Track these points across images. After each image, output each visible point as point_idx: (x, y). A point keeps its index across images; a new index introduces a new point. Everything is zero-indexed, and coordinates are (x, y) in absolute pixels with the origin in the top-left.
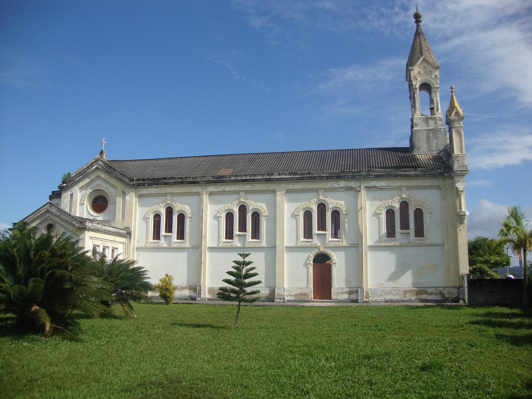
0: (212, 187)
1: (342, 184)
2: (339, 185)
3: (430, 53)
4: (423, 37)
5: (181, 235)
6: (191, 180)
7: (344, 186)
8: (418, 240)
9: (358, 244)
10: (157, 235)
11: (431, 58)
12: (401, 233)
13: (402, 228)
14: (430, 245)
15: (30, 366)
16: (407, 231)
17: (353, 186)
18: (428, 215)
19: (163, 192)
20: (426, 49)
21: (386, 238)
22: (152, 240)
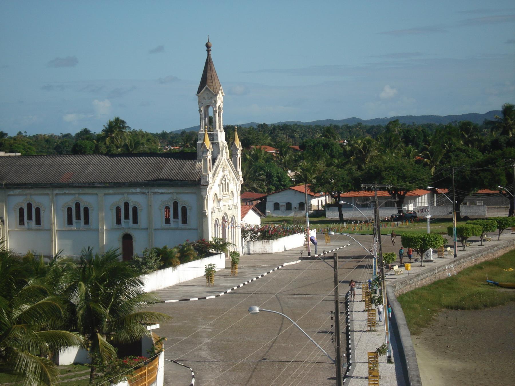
0: (57, 190)
1: (138, 190)
2: (136, 191)
3: (212, 82)
4: (210, 66)
5: (184, 221)
6: (77, 185)
7: (139, 191)
8: (184, 226)
9: (147, 228)
10: (70, 222)
11: (212, 87)
12: (174, 222)
13: (174, 218)
14: (190, 229)
15: (463, 275)
16: (177, 220)
17: (145, 192)
18: (189, 210)
19: (24, 193)
20: (210, 78)
21: (67, 225)
22: (164, 224)
